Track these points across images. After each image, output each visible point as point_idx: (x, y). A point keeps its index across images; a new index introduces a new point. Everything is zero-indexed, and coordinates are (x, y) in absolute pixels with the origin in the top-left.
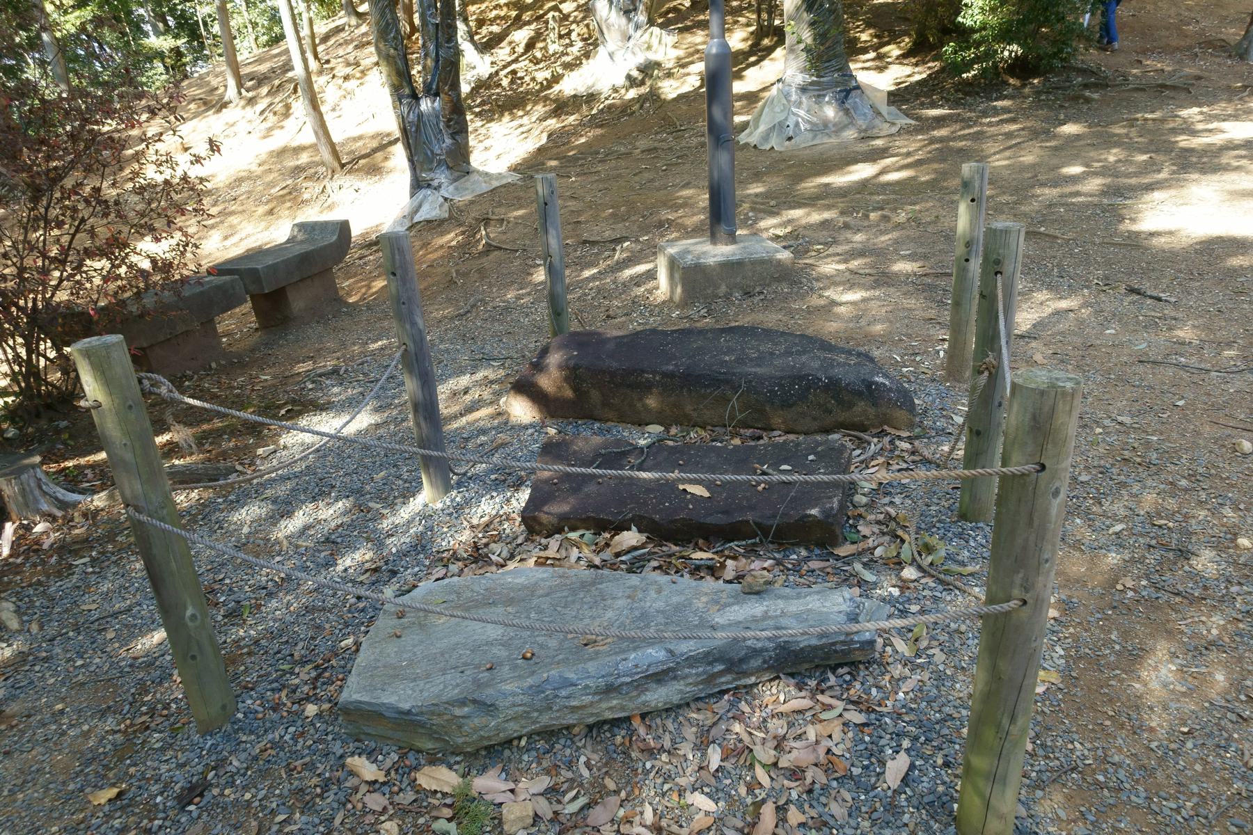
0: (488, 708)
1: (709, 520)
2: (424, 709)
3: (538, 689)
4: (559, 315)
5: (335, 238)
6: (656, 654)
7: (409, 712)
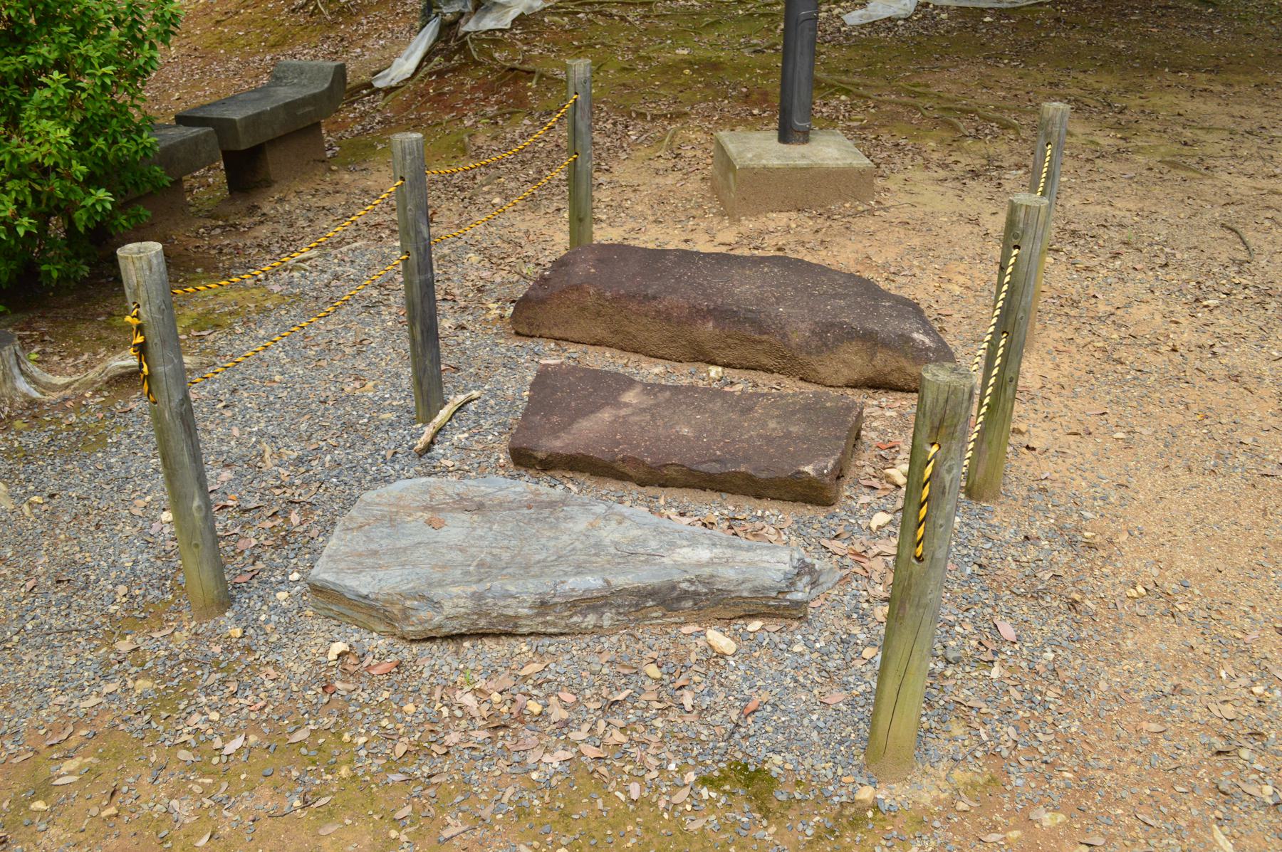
0: (436, 605)
1: (703, 468)
2: (380, 597)
3: (478, 597)
4: (581, 220)
5: (326, 85)
6: (592, 582)
7: (366, 597)
